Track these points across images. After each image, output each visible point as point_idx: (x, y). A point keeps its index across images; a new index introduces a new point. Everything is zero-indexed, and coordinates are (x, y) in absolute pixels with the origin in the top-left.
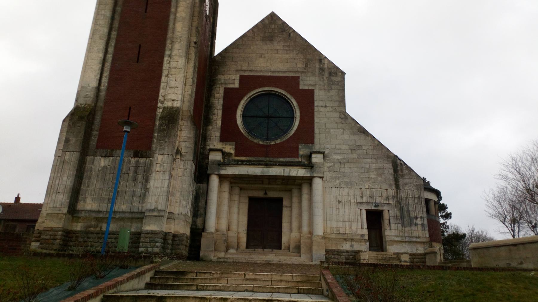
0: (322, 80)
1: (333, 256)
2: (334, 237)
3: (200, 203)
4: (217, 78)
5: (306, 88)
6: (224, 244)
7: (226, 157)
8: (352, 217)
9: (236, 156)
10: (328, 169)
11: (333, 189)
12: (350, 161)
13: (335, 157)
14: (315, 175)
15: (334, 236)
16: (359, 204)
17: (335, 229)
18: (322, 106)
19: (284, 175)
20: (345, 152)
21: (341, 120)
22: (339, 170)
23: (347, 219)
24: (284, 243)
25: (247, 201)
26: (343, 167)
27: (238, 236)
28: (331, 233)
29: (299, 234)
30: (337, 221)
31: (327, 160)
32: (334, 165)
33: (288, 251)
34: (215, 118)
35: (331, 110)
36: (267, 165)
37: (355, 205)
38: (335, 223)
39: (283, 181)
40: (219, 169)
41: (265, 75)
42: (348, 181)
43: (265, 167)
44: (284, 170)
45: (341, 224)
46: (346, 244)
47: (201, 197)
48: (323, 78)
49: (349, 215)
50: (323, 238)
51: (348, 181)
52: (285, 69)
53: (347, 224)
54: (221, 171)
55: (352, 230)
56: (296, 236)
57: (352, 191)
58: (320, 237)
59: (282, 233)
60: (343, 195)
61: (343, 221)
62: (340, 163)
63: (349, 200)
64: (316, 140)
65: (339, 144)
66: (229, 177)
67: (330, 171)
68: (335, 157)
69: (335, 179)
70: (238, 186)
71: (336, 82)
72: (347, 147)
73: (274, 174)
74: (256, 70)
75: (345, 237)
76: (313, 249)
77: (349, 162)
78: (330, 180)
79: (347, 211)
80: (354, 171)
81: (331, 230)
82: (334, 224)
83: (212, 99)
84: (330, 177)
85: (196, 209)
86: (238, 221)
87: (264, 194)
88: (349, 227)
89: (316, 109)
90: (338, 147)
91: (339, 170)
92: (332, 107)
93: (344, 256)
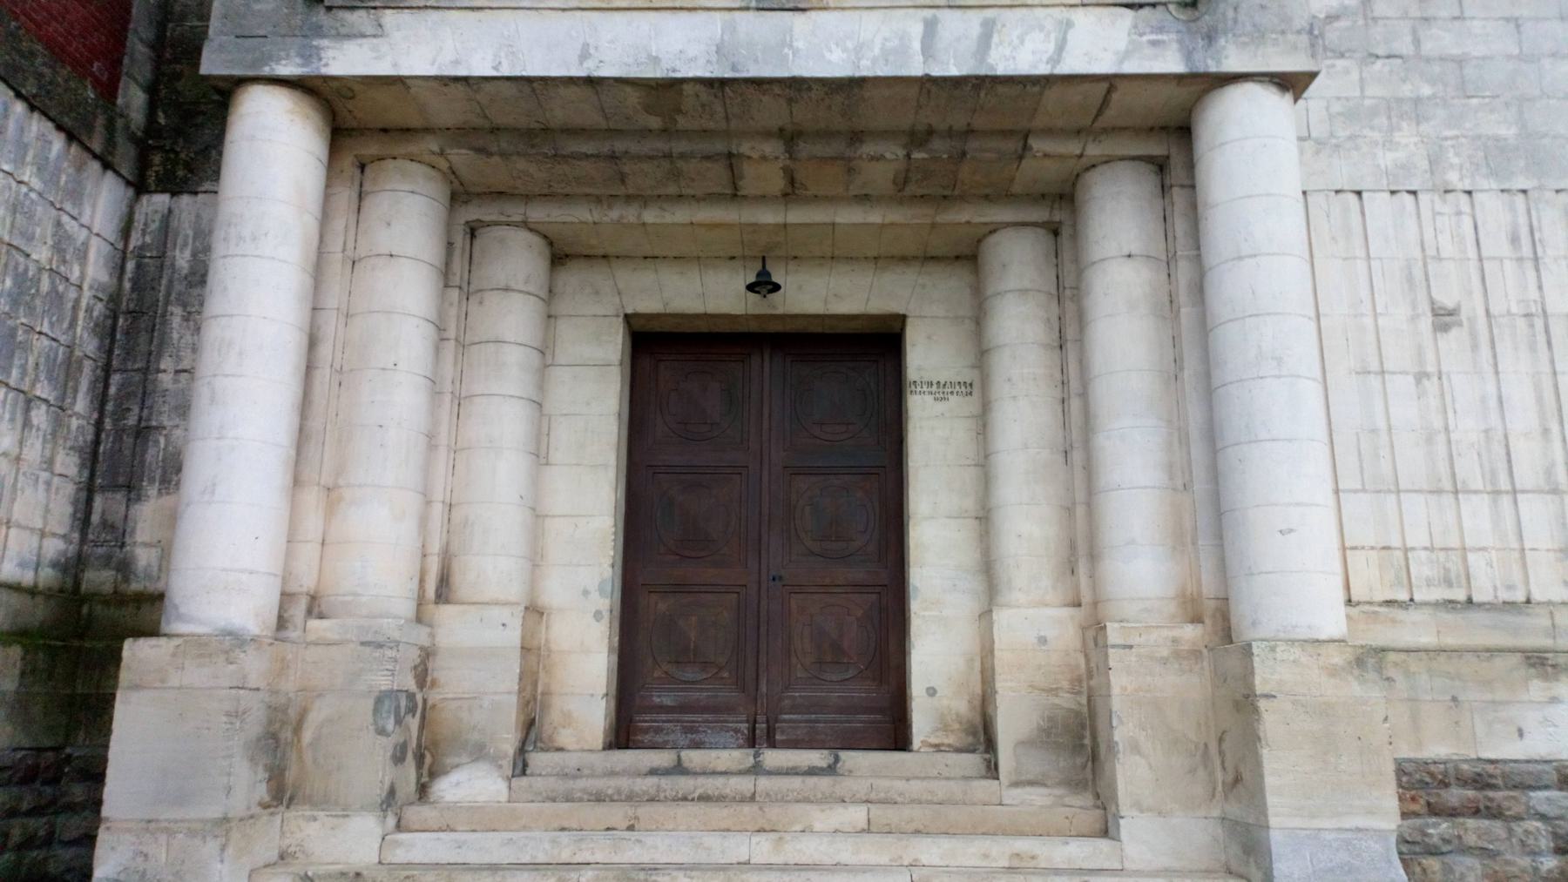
2: (1427, 639)
3: (166, 363)
6: (381, 732)
11: (1378, 204)
14: (1233, 62)
15: (1417, 631)
17: (1422, 568)
19: (936, 72)
22: (1417, 42)
24: (932, 692)
25: (613, 347)
26: (1444, 13)
27: (525, 649)
28: (1389, 603)
29: (1067, 612)
30: (1439, 492)
33: (973, 761)
38: (1416, 507)
39: (917, 155)
40: (318, 31)
42: (1508, 132)
44: (930, 28)
46: (1554, 700)
47: (177, 311)
49: (1546, 431)
50: (1360, 662)
51: (1503, 131)
54: (329, 54)
56: (1050, 633)
58: (1337, 658)
60: (1472, 253)
61: (1496, 493)
63: (1533, 293)
66: (428, 130)
69: (1382, 121)
70: (525, 225)
73: (833, 63)
76: (1270, 781)
78: (1342, 133)
79: (1520, 394)
84: (1337, 108)
85: (132, 420)
86: (537, 516)
87: (751, 288)
91: (1417, 42)
93: (1543, 817)
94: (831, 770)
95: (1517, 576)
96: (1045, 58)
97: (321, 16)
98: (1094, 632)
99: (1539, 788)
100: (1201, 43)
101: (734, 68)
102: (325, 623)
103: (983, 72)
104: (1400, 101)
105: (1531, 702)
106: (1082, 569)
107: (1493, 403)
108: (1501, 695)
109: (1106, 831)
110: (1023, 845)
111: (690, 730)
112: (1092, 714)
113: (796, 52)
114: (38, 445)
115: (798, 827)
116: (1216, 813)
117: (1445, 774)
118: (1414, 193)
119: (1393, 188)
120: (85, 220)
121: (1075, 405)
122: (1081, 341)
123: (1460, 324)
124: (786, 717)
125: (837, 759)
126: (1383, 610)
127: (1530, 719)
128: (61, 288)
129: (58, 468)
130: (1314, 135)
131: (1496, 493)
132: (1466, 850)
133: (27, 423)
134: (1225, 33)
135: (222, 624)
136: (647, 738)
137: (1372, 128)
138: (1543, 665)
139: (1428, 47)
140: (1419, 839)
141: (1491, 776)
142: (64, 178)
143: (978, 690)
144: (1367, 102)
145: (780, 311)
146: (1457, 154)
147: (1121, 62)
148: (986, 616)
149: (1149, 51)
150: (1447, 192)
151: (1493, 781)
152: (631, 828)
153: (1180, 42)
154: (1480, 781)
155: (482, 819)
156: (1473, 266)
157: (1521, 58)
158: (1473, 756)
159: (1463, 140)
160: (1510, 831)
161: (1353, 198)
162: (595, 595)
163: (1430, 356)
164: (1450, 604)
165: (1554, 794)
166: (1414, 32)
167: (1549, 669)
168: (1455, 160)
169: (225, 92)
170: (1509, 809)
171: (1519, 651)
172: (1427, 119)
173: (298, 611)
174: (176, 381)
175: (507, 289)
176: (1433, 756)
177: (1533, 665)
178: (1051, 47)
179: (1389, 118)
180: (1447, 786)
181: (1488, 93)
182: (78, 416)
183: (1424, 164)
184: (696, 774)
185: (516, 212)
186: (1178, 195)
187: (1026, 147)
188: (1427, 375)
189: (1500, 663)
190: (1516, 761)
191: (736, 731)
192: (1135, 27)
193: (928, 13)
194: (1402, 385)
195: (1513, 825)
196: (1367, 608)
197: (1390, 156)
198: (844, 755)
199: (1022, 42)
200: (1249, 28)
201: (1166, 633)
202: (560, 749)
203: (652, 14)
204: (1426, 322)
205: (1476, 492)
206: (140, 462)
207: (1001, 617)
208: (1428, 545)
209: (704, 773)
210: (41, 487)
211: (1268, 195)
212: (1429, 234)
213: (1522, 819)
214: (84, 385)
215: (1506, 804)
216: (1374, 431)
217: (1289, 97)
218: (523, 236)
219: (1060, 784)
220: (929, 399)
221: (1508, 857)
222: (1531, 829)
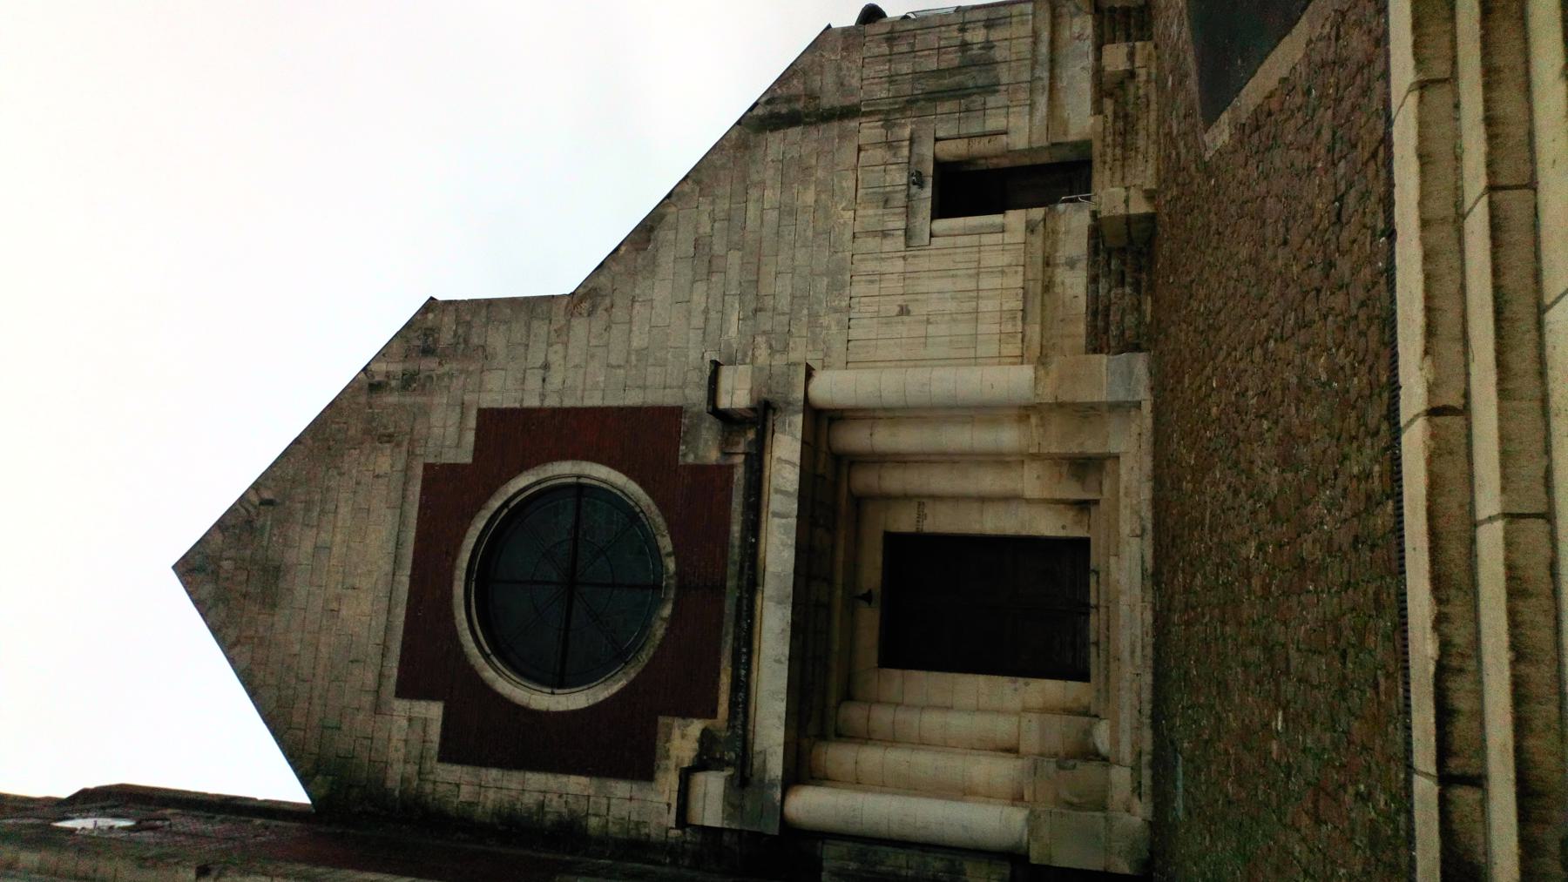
1: (1113, 330)
2: (1037, 328)
3: (904, 872)
6: (1074, 767)
11: (853, 334)
13: (733, 330)
14: (800, 395)
15: (1034, 331)
17: (1009, 328)
18: (544, 380)
19: (795, 513)
21: (600, 311)
22: (784, 314)
23: (971, 285)
24: (1064, 527)
28: (1023, 341)
33: (1093, 509)
38: (982, 328)
40: (762, 780)
42: (826, 280)
45: (988, 305)
46: (1063, 283)
47: (878, 868)
49: (953, 276)
51: (825, 283)
53: (987, 282)
58: (1042, 372)
60: (877, 299)
63: (895, 276)
64: (669, 399)
71: (460, 331)
72: (701, 287)
75: (1039, 289)
79: (938, 285)
82: (988, 327)
84: (810, 347)
90: (698, 321)
91: (784, 314)
93: (1110, 291)
94: (1097, 573)
95: (1013, 292)
97: (755, 779)
98: (1035, 457)
100: (791, 407)
102: (1026, 793)
103: (797, 494)
104: (809, 322)
106: (1008, 459)
107: (941, 296)
108: (1060, 303)
109: (1117, 457)
112: (1070, 459)
116: (1108, 414)
118: (850, 319)
121: (932, 458)
122: (904, 455)
123: (907, 306)
125: (1093, 571)
127: (1070, 292)
131: (978, 297)
132: (1122, 320)
139: (787, 310)
143: (1062, 506)
148: (1029, 501)
156: (882, 299)
160: (1115, 303)
161: (851, 344)
162: (1018, 685)
163: (921, 318)
164: (1024, 319)
166: (779, 314)
169: (785, 823)
174: (911, 868)
186: (846, 414)
188: (928, 319)
193: (770, 515)
194: (931, 329)
197: (833, 328)
201: (1034, 429)
204: (906, 318)
206: (1026, 156)
207: (1028, 494)
212: (868, 315)
216: (951, 341)
217: (814, 373)
219: (1101, 475)
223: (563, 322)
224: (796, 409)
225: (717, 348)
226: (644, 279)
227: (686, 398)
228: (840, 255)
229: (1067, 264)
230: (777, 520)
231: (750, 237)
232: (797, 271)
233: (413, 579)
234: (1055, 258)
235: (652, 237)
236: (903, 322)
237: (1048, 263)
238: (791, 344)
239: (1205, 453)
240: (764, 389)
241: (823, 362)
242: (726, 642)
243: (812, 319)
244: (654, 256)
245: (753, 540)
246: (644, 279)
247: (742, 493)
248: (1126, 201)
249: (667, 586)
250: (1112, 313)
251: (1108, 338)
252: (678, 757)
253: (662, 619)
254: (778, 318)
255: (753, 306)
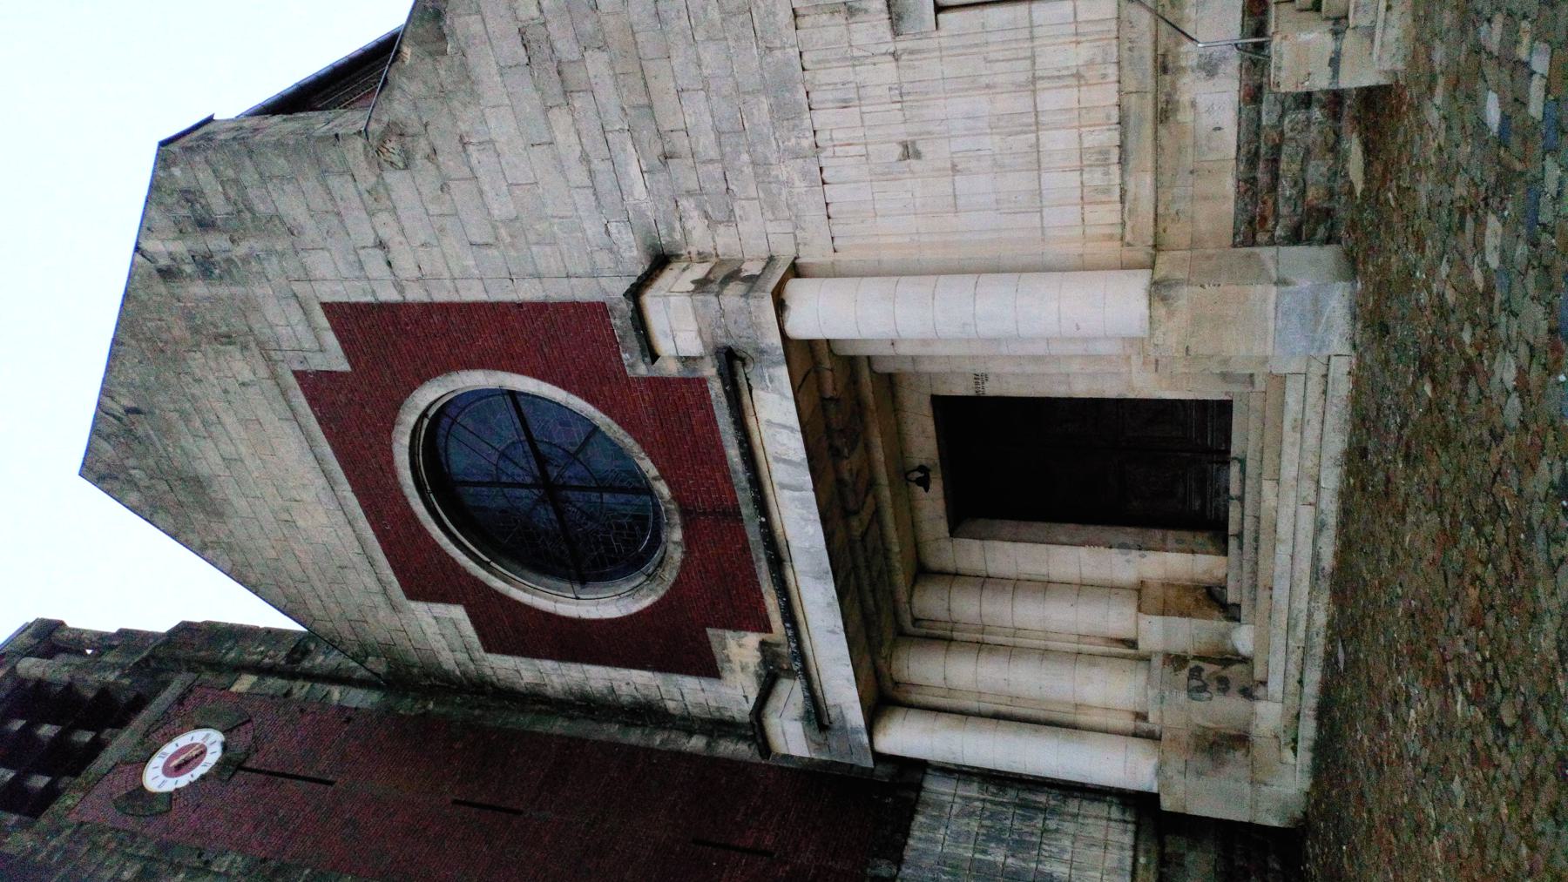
0: (255, 267)
1: (1286, 189)
2: (1148, 179)
4: (458, 673)
5: (331, 340)
6: (1210, 699)
7: (785, 667)
8: (998, 67)
9: (767, 628)
10: (721, 229)
12: (643, 100)
13: (638, 190)
14: (777, 341)
15: (1142, 186)
16: (904, 26)
18: (389, 264)
19: (811, 486)
20: (597, 133)
21: (419, 160)
23: (1023, 103)
31: (670, 235)
32: (689, 193)
34: (624, 687)
35: (384, 217)
36: (778, 561)
37: (912, 52)
38: (1051, 180)
40: (843, 728)
41: (359, 511)
43: (788, 564)
45: (1058, 141)
46: (1193, 104)
48: (246, 260)
51: (765, 107)
52: (289, 429)
53: (1053, 100)
55: (1091, 63)
57: (822, 76)
58: (1161, 311)
59: (1131, 396)
62: (666, 157)
64: (583, 292)
65: (562, 170)
67: (730, 218)
68: (639, 191)
70: (910, 602)
71: (232, 194)
72: (561, 119)
74: (357, 543)
75: (1149, 112)
77: (651, 107)
78: (787, 214)
80: (693, 70)
81: (1104, 198)
82: (1059, 182)
83: (549, 691)
84: (769, 215)
88: (1074, 82)
89: (415, 294)
90: (578, 175)
91: (711, 161)
92: (371, 214)
93: (1282, 117)
94: (1242, 462)
96: (791, 434)
97: (836, 725)
99: (1260, 119)
101: (827, 573)
103: (806, 463)
105: (1195, 121)
108: (1189, 141)
110: (1287, 425)
111: (1218, 494)
113: (812, 547)
114: (1066, 824)
115: (1274, 514)
117: (1246, 181)
119: (821, 183)
120: (950, 799)
123: (913, 143)
124: (1209, 443)
125: (1236, 458)
126: (1127, 205)
127: (1207, 122)
128: (988, 813)
129: (1076, 811)
130: (791, 230)
133: (1057, 831)
134: (756, 343)
135: (1153, 776)
136: (1222, 515)
137: (780, 194)
138: (1166, 111)
139: (713, 153)
140: (1292, 202)
141: (1249, 152)
142: (934, 813)
144: (762, 195)
145: (937, 461)
146: (789, 140)
147: (787, 398)
149: (777, 383)
150: (817, 146)
151: (1253, 150)
152: (1271, 589)
153: (768, 367)
154: (1252, 159)
155: (1263, 642)
157: (706, 89)
158: (1234, 162)
159: (777, 135)
164: (1122, 161)
165: (1264, 107)
167: (1170, 107)
168: (793, 141)
170: (1274, 140)
171: (1156, 132)
172: (766, 158)
173: (1144, 726)
175: (949, 610)
176: (1233, 189)
177: (1167, 118)
178: (785, 432)
179: (770, 183)
180: (1255, 178)
181: (739, 115)
182: (1048, 800)
183: (800, 161)
184: (1243, 527)
185: (903, 606)
187: (831, 399)
189: (1165, 141)
190: (1239, 133)
191: (1218, 470)
192: (763, 389)
195: (1286, 136)
196: (1126, 216)
197: (797, 183)
198: (1233, 455)
199: (785, 445)
200: (751, 331)
202: (1227, 575)
203: (804, 604)
205: (1038, 139)
208: (1078, 173)
209: (1243, 524)
210: (1087, 821)
211: (857, 323)
213: (1282, 131)
214: (1031, 797)
215: (1270, 144)
218: (915, 600)
220: (986, 384)
221: (1310, 141)
222: (1290, 126)
223: (373, 179)
224: (775, 359)
225: (624, 217)
226: (465, 105)
227: (603, 290)
228: (778, 53)
229: (1200, 67)
230: (787, 493)
231: (611, 23)
232: (712, 87)
233: (356, 492)
234: (1177, 57)
235: (446, 30)
236: (912, 172)
237: (1163, 66)
238: (738, 212)
239: (1451, 670)
240: (719, 332)
241: (795, 237)
242: (760, 567)
243: (761, 171)
244: (464, 65)
245: (763, 519)
246: (465, 105)
247: (727, 412)
248: (1335, 62)
249: (666, 511)
250: (1283, 157)
251: (1275, 203)
252: (741, 662)
253: (675, 543)
254: (702, 169)
255: (658, 150)
